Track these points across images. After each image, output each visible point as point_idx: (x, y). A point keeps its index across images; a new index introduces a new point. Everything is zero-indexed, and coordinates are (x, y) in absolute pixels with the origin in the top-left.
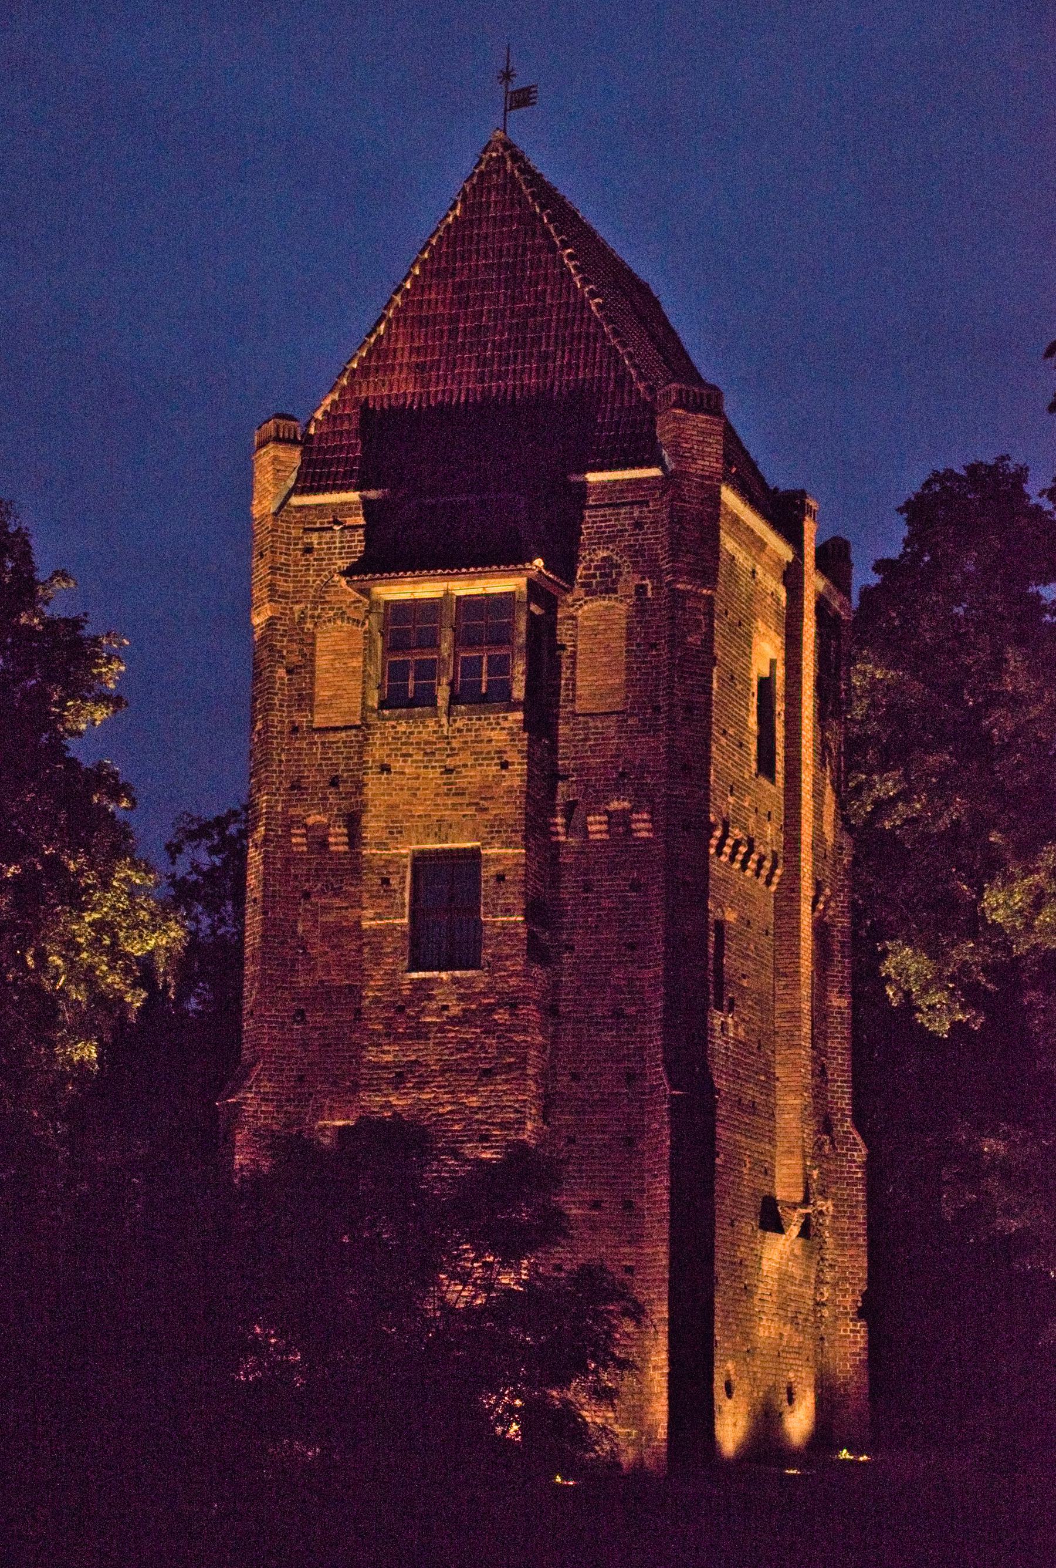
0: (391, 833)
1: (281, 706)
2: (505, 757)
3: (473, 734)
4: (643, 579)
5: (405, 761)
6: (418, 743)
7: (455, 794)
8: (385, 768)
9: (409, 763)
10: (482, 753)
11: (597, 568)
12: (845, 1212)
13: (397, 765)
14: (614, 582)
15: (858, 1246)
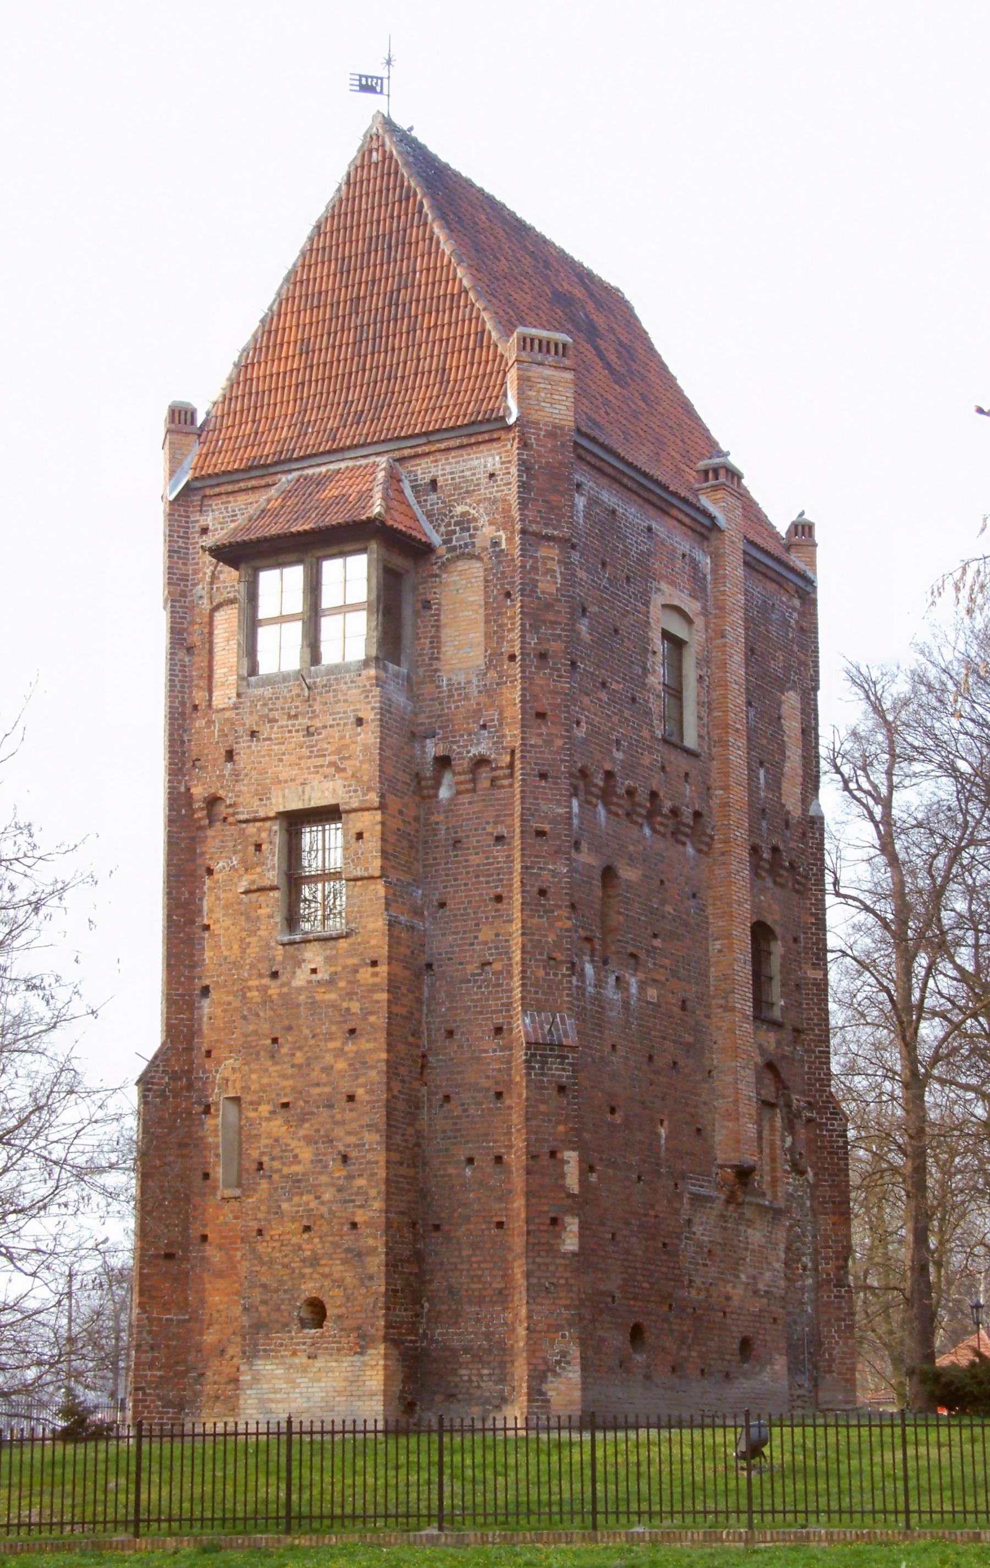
0: (261, 800)
1: (182, 687)
4: (498, 530)
5: (272, 728)
6: (283, 709)
7: (316, 756)
8: (253, 734)
11: (456, 524)
13: (265, 731)
14: (472, 536)
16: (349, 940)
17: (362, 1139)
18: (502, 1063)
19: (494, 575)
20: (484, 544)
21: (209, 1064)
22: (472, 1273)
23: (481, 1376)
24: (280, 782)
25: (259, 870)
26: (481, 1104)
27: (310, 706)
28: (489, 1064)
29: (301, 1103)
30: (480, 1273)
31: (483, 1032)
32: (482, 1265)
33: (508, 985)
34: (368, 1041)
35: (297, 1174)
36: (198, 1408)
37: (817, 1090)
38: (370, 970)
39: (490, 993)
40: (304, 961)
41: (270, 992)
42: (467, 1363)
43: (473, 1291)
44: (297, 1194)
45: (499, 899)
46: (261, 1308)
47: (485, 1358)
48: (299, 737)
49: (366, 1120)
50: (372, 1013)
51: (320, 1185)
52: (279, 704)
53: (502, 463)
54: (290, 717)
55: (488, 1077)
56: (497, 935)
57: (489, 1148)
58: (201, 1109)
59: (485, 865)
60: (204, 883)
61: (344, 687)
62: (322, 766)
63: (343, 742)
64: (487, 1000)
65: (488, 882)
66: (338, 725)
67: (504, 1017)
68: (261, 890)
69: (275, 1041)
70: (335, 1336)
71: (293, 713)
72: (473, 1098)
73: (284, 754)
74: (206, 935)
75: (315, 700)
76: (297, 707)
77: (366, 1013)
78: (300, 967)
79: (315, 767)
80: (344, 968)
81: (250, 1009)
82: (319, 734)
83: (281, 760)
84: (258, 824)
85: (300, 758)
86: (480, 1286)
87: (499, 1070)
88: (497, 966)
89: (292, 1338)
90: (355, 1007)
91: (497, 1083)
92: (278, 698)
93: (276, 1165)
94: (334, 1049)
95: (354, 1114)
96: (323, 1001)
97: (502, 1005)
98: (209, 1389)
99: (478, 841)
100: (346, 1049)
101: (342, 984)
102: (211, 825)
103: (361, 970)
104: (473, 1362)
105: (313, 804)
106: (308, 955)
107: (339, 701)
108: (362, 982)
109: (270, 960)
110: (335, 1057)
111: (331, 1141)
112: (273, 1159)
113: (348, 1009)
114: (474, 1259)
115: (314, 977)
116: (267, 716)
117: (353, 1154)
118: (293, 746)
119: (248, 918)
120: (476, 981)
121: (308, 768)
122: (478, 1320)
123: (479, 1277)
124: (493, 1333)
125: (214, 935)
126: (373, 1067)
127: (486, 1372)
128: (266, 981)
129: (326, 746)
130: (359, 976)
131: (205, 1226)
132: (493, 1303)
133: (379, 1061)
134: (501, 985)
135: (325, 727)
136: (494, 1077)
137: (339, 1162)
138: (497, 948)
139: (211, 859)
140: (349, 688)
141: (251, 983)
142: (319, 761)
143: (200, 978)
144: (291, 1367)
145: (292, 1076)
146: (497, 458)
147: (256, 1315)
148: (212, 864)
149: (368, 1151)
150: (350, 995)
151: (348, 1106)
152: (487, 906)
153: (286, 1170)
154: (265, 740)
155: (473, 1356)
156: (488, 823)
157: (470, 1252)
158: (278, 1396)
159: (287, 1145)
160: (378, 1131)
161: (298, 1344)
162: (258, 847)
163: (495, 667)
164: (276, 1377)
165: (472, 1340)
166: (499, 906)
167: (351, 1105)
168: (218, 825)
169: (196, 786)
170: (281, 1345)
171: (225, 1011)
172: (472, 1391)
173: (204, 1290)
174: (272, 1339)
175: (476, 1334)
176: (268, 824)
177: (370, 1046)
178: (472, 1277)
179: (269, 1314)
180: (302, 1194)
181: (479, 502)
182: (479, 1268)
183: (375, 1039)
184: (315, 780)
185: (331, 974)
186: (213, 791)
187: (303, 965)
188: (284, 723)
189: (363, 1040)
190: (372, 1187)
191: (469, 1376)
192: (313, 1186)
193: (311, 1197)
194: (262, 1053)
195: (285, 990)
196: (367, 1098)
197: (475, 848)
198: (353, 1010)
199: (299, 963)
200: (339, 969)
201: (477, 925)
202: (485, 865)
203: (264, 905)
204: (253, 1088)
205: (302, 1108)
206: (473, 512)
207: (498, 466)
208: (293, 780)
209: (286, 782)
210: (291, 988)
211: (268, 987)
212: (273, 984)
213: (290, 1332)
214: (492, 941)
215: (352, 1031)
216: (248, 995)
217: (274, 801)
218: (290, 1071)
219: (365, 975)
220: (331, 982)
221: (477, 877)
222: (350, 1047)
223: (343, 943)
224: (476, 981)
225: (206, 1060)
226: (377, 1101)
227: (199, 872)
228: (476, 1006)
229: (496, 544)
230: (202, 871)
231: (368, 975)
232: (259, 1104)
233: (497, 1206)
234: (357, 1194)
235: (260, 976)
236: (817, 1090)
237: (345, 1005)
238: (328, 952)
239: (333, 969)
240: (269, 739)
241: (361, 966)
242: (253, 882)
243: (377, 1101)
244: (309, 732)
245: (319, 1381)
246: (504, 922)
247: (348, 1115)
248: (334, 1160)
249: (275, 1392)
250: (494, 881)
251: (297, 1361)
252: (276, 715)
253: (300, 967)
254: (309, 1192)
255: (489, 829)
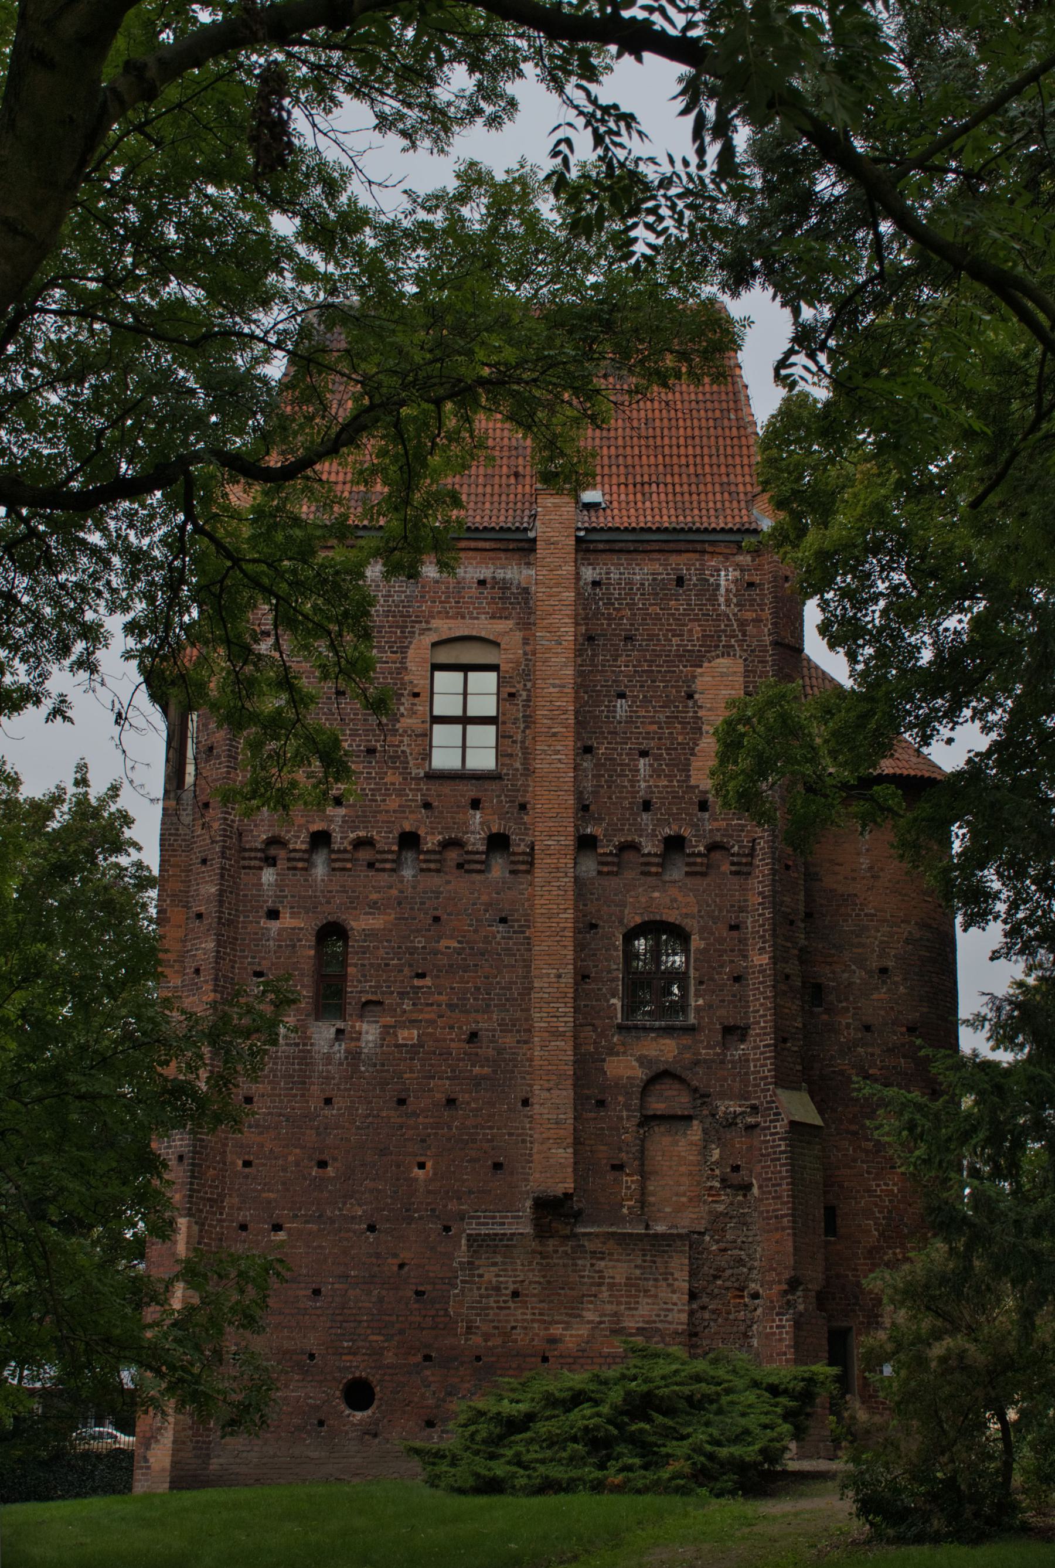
12: (770, 1192)
15: (784, 1229)
37: (763, 1091)
236: (763, 1091)
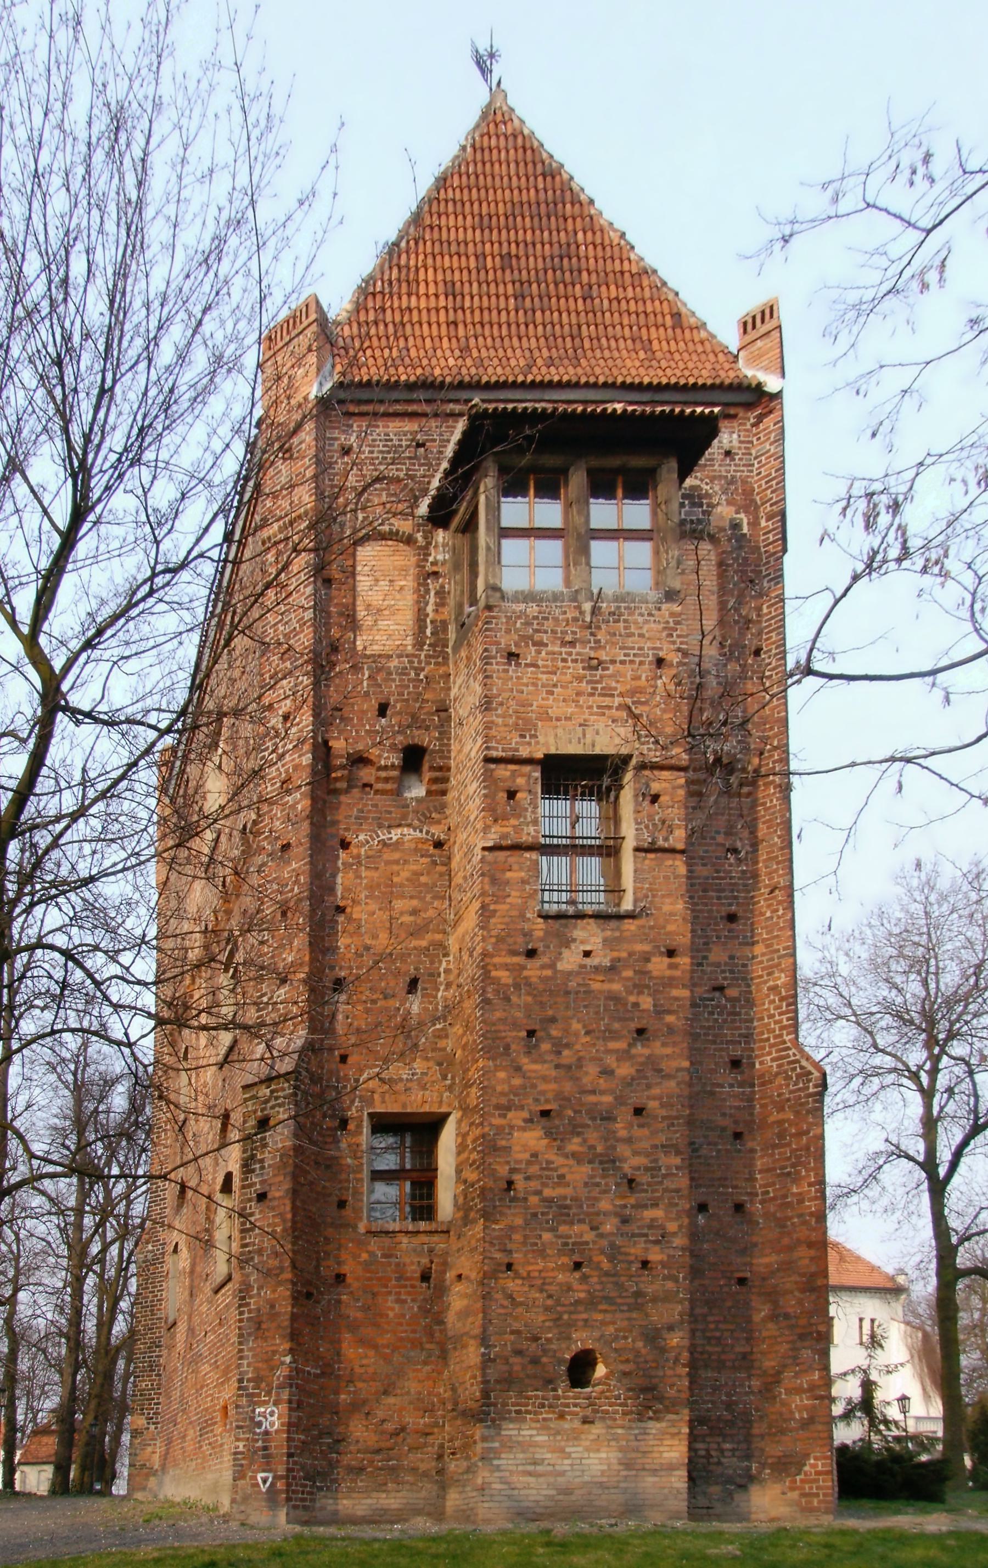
0: (523, 736)
2: (661, 654)
3: (622, 624)
4: (737, 512)
5: (539, 652)
7: (600, 695)
8: (512, 656)
9: (543, 653)
10: (633, 648)
13: (530, 654)
16: (637, 922)
17: (656, 1161)
18: (742, 1100)
19: (735, 559)
20: (721, 524)
21: (343, 1070)
22: (708, 1334)
23: (722, 1451)
24: (551, 719)
25: (513, 822)
26: (716, 1144)
27: (592, 634)
28: (724, 1100)
29: (570, 1113)
30: (718, 1334)
31: (716, 1064)
32: (722, 1326)
33: (747, 1014)
34: (664, 1045)
35: (565, 1198)
36: (335, 1481)
38: (666, 960)
39: (725, 1021)
40: (574, 940)
41: (525, 973)
42: (704, 1436)
43: (710, 1354)
44: (565, 1222)
45: (732, 918)
46: (511, 1360)
47: (727, 1431)
48: (579, 669)
49: (662, 1139)
50: (669, 1012)
51: (598, 1214)
52: (548, 625)
53: (741, 442)
54: (564, 644)
55: (724, 1115)
56: (732, 957)
57: (727, 1194)
58: (336, 1123)
59: (714, 878)
60: (337, 857)
61: (640, 619)
62: (609, 708)
63: (637, 683)
64: (721, 1028)
65: (719, 898)
66: (632, 662)
67: (743, 1050)
68: (517, 847)
69: (531, 1033)
70: (618, 1397)
71: (569, 638)
72: (705, 1137)
73: (555, 686)
74: (341, 918)
75: (599, 628)
76: (574, 633)
77: (660, 1012)
78: (568, 947)
79: (599, 707)
80: (630, 954)
81: (497, 992)
82: (604, 669)
83: (552, 693)
84: (512, 767)
85: (578, 694)
86: (718, 1349)
87: (738, 1108)
88: (732, 992)
89: (557, 1398)
90: (647, 1002)
91: (736, 1122)
92: (547, 619)
93: (534, 1185)
94: (617, 1051)
95: (645, 1131)
96: (600, 992)
97: (740, 1035)
98: (346, 1460)
99: (706, 851)
100: (633, 1051)
101: (628, 973)
102: (347, 791)
103: (654, 959)
104: (710, 1435)
105: (597, 751)
106: (578, 933)
107: (632, 635)
108: (655, 974)
109: (525, 935)
110: (618, 1060)
111: (614, 1161)
112: (528, 1178)
113: (636, 1005)
114: (710, 1318)
115: (588, 961)
116: (531, 637)
117: (644, 1179)
118: (569, 677)
119: (494, 881)
120: (706, 1006)
121: (590, 707)
122: (715, 1389)
123: (718, 1339)
124: (736, 1403)
125: (350, 919)
126: (669, 1077)
127: (728, 1446)
128: (520, 960)
129: (614, 684)
130: (650, 966)
131: (339, 1263)
132: (735, 1369)
133: (678, 1070)
134: (739, 1014)
135: (613, 662)
136: (731, 1115)
137: (625, 1188)
138: (732, 972)
139: (347, 829)
140: (647, 622)
141: (496, 960)
142: (607, 701)
143: (332, 968)
144: (558, 1433)
145: (556, 1080)
146: (735, 436)
147: (505, 1368)
148: (349, 836)
149: (665, 1176)
150: (639, 988)
151: (636, 1120)
152: (716, 924)
153: (547, 1192)
154: (527, 665)
155: (711, 1428)
156: (718, 832)
157: (706, 1310)
158: (539, 1468)
159: (548, 1162)
160: (678, 1153)
161: (567, 1405)
162: (511, 795)
163: (738, 659)
164: (536, 1445)
165: (708, 1410)
166: (734, 926)
167: (641, 1120)
168: (356, 792)
169: (338, 738)
170: (543, 1406)
171: (367, 1011)
172: (712, 1467)
173: (339, 1341)
174: (529, 1398)
175: (713, 1403)
176: (527, 769)
177: (668, 1051)
178: (709, 1339)
179: (524, 1368)
180: (572, 1223)
181: (712, 479)
182: (717, 1329)
183: (675, 1044)
184: (601, 724)
185: (612, 960)
186: (360, 747)
187: (573, 946)
188: (557, 649)
189: (658, 1044)
190: (671, 1220)
191: (707, 1450)
192: (588, 1214)
193: (585, 1227)
194: (513, 1047)
195: (548, 973)
196: (664, 1112)
197: (702, 858)
198: (643, 1006)
199: (567, 943)
200: (624, 955)
201: (706, 944)
202: (714, 878)
203: (515, 867)
204: (499, 1089)
205: (570, 1119)
206: (705, 487)
207: (735, 443)
208: (568, 719)
209: (558, 719)
210: (556, 971)
211: (524, 968)
212: (530, 963)
213: (555, 1390)
214: (726, 964)
215: (640, 1032)
216: (494, 974)
217: (541, 739)
218: (553, 1073)
219: (659, 965)
220: (612, 969)
221: (705, 891)
222: (639, 1049)
223: (630, 926)
224: (706, 1006)
225: (342, 1065)
226: (677, 1118)
227: (330, 843)
228: (708, 1035)
229: (736, 526)
230: (335, 842)
231: (665, 966)
232: (508, 1109)
233: (739, 1260)
234: (650, 1227)
235: (514, 953)
237: (632, 999)
238: (609, 933)
239: (615, 954)
240: (535, 665)
241: (654, 955)
242: (504, 836)
243: (677, 1118)
244: (594, 665)
245: (598, 1451)
246: (740, 944)
247: (637, 1132)
248: (617, 1185)
249: (535, 1464)
250: (726, 898)
251: (567, 1425)
252: (545, 638)
253: (568, 947)
254: (581, 1221)
255: (720, 839)
